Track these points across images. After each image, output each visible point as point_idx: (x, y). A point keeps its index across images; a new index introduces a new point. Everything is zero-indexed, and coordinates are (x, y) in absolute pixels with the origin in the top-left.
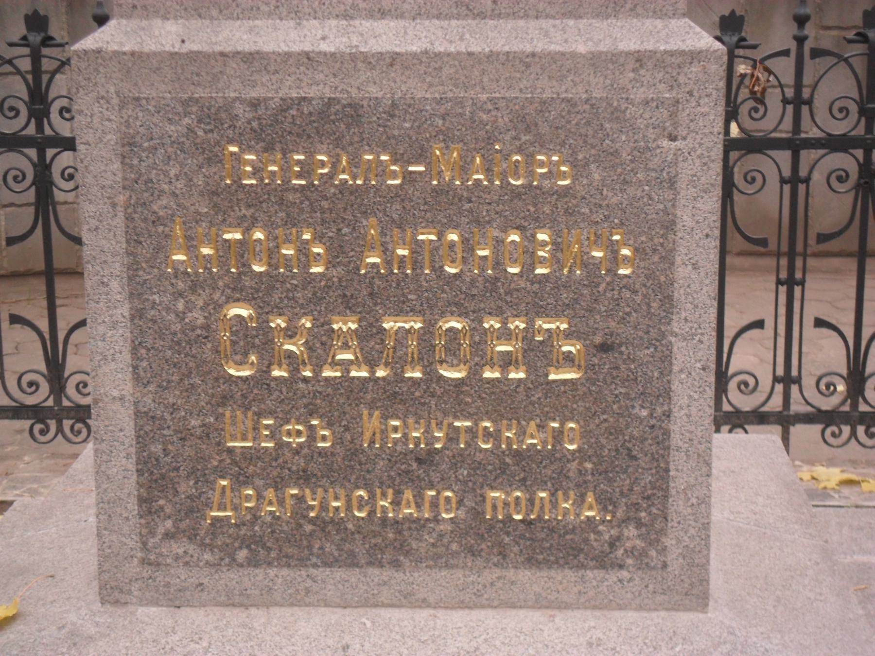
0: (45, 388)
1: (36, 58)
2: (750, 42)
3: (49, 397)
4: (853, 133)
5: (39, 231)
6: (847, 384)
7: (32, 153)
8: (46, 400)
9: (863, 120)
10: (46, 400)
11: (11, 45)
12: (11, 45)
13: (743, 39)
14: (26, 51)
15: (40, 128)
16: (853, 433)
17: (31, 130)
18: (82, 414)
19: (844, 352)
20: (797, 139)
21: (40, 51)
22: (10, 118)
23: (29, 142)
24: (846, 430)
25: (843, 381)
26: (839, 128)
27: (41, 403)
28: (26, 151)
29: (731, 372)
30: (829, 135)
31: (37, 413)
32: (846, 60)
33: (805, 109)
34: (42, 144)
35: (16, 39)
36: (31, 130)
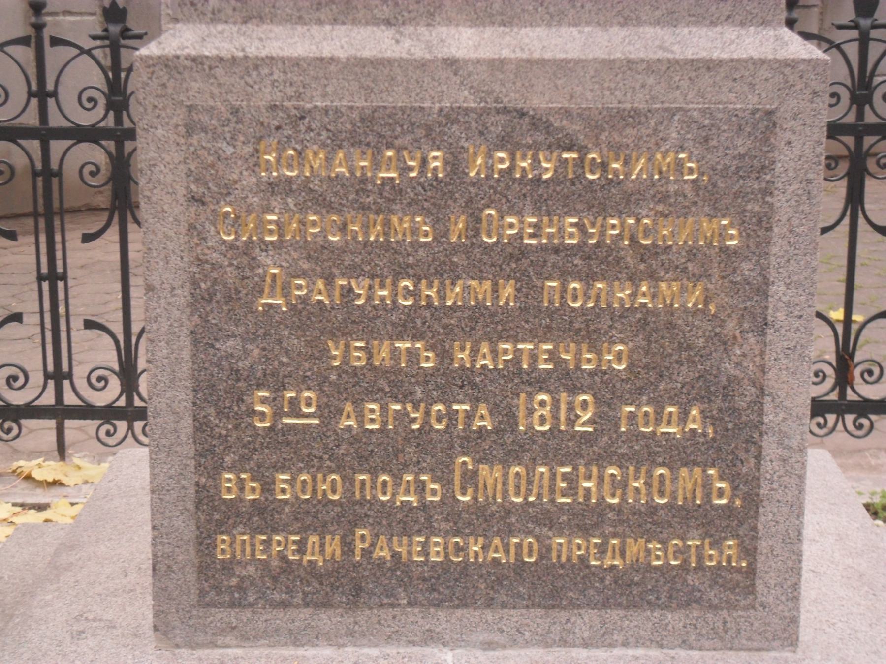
0: (115, 385)
1: (864, 42)
2: (137, 31)
3: (120, 396)
4: (102, 125)
5: (846, 221)
6: (120, 379)
7: (111, 145)
8: (117, 400)
9: (855, 106)
10: (117, 400)
11: (840, 27)
12: (840, 27)
13: (128, 30)
14: (855, 34)
15: (118, 120)
16: (130, 428)
17: (110, 122)
18: (141, 414)
19: (832, 340)
20: (861, 125)
21: (868, 34)
22: (88, 110)
23: (107, 134)
24: (122, 425)
25: (116, 377)
26: (85, 119)
27: (114, 402)
28: (843, 138)
29: (857, 359)
30: (78, 125)
31: (108, 414)
32: (838, 47)
33: (51, 102)
34: (859, 131)
35: (844, 21)
36: (110, 122)
